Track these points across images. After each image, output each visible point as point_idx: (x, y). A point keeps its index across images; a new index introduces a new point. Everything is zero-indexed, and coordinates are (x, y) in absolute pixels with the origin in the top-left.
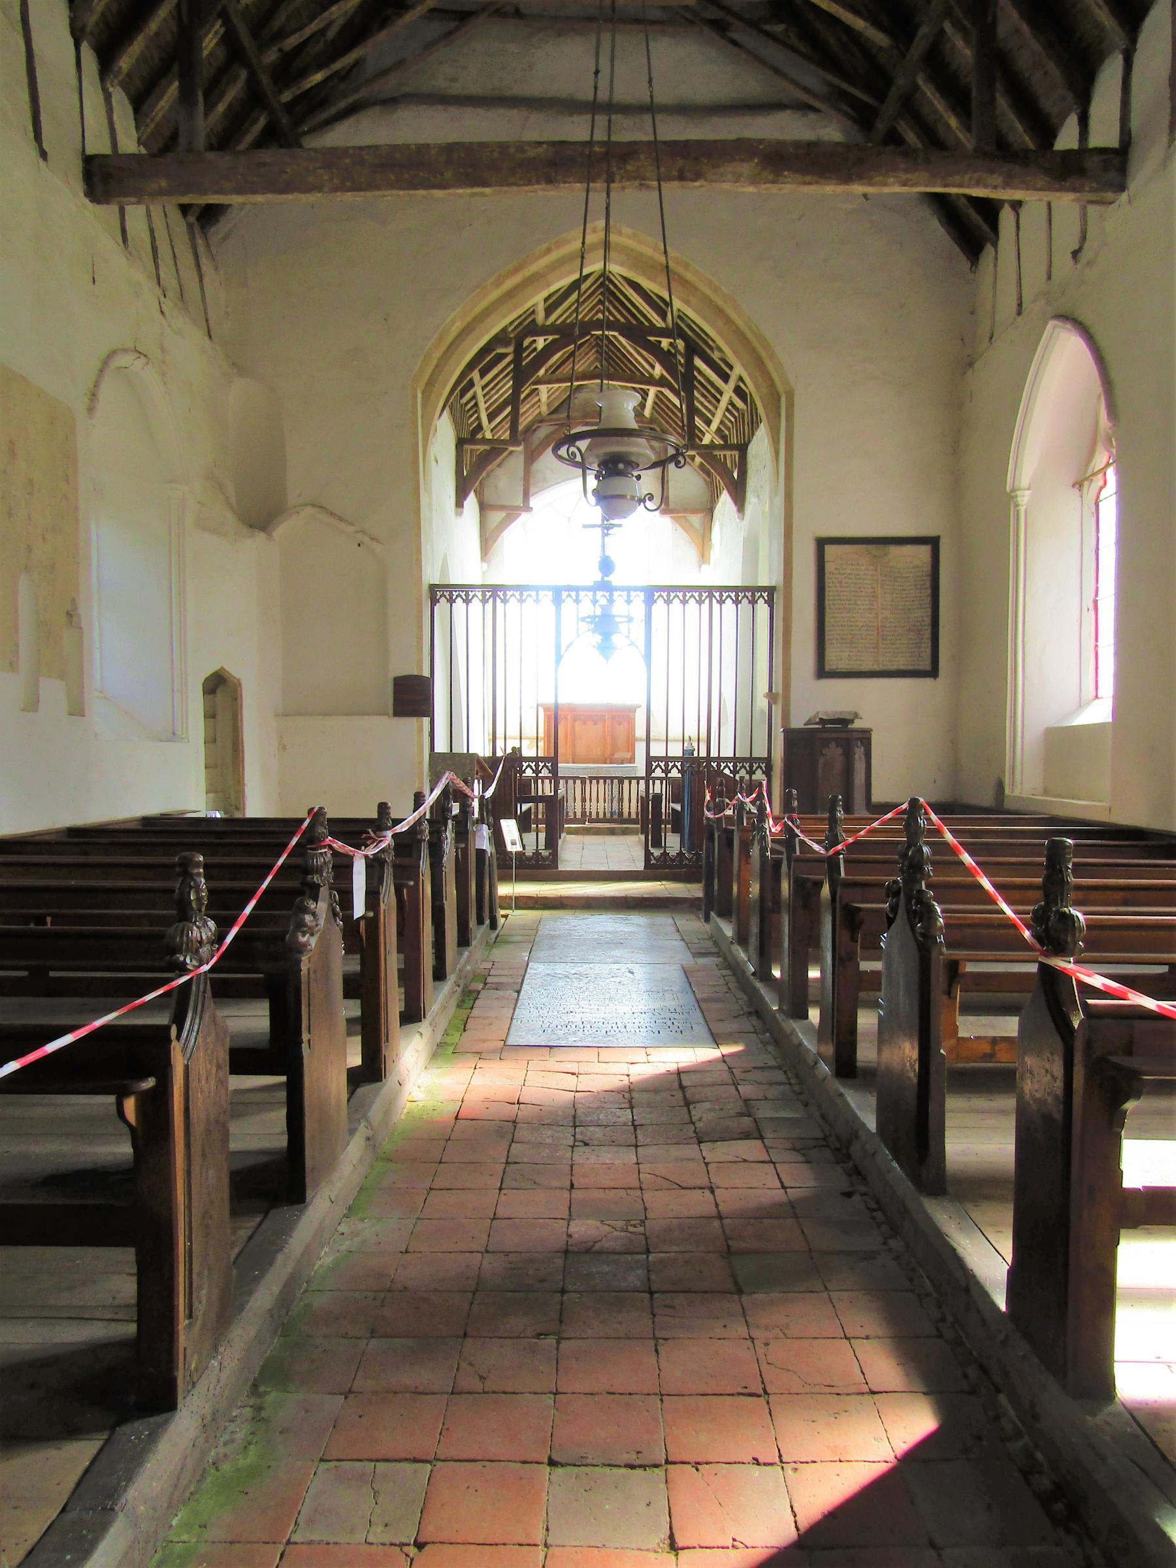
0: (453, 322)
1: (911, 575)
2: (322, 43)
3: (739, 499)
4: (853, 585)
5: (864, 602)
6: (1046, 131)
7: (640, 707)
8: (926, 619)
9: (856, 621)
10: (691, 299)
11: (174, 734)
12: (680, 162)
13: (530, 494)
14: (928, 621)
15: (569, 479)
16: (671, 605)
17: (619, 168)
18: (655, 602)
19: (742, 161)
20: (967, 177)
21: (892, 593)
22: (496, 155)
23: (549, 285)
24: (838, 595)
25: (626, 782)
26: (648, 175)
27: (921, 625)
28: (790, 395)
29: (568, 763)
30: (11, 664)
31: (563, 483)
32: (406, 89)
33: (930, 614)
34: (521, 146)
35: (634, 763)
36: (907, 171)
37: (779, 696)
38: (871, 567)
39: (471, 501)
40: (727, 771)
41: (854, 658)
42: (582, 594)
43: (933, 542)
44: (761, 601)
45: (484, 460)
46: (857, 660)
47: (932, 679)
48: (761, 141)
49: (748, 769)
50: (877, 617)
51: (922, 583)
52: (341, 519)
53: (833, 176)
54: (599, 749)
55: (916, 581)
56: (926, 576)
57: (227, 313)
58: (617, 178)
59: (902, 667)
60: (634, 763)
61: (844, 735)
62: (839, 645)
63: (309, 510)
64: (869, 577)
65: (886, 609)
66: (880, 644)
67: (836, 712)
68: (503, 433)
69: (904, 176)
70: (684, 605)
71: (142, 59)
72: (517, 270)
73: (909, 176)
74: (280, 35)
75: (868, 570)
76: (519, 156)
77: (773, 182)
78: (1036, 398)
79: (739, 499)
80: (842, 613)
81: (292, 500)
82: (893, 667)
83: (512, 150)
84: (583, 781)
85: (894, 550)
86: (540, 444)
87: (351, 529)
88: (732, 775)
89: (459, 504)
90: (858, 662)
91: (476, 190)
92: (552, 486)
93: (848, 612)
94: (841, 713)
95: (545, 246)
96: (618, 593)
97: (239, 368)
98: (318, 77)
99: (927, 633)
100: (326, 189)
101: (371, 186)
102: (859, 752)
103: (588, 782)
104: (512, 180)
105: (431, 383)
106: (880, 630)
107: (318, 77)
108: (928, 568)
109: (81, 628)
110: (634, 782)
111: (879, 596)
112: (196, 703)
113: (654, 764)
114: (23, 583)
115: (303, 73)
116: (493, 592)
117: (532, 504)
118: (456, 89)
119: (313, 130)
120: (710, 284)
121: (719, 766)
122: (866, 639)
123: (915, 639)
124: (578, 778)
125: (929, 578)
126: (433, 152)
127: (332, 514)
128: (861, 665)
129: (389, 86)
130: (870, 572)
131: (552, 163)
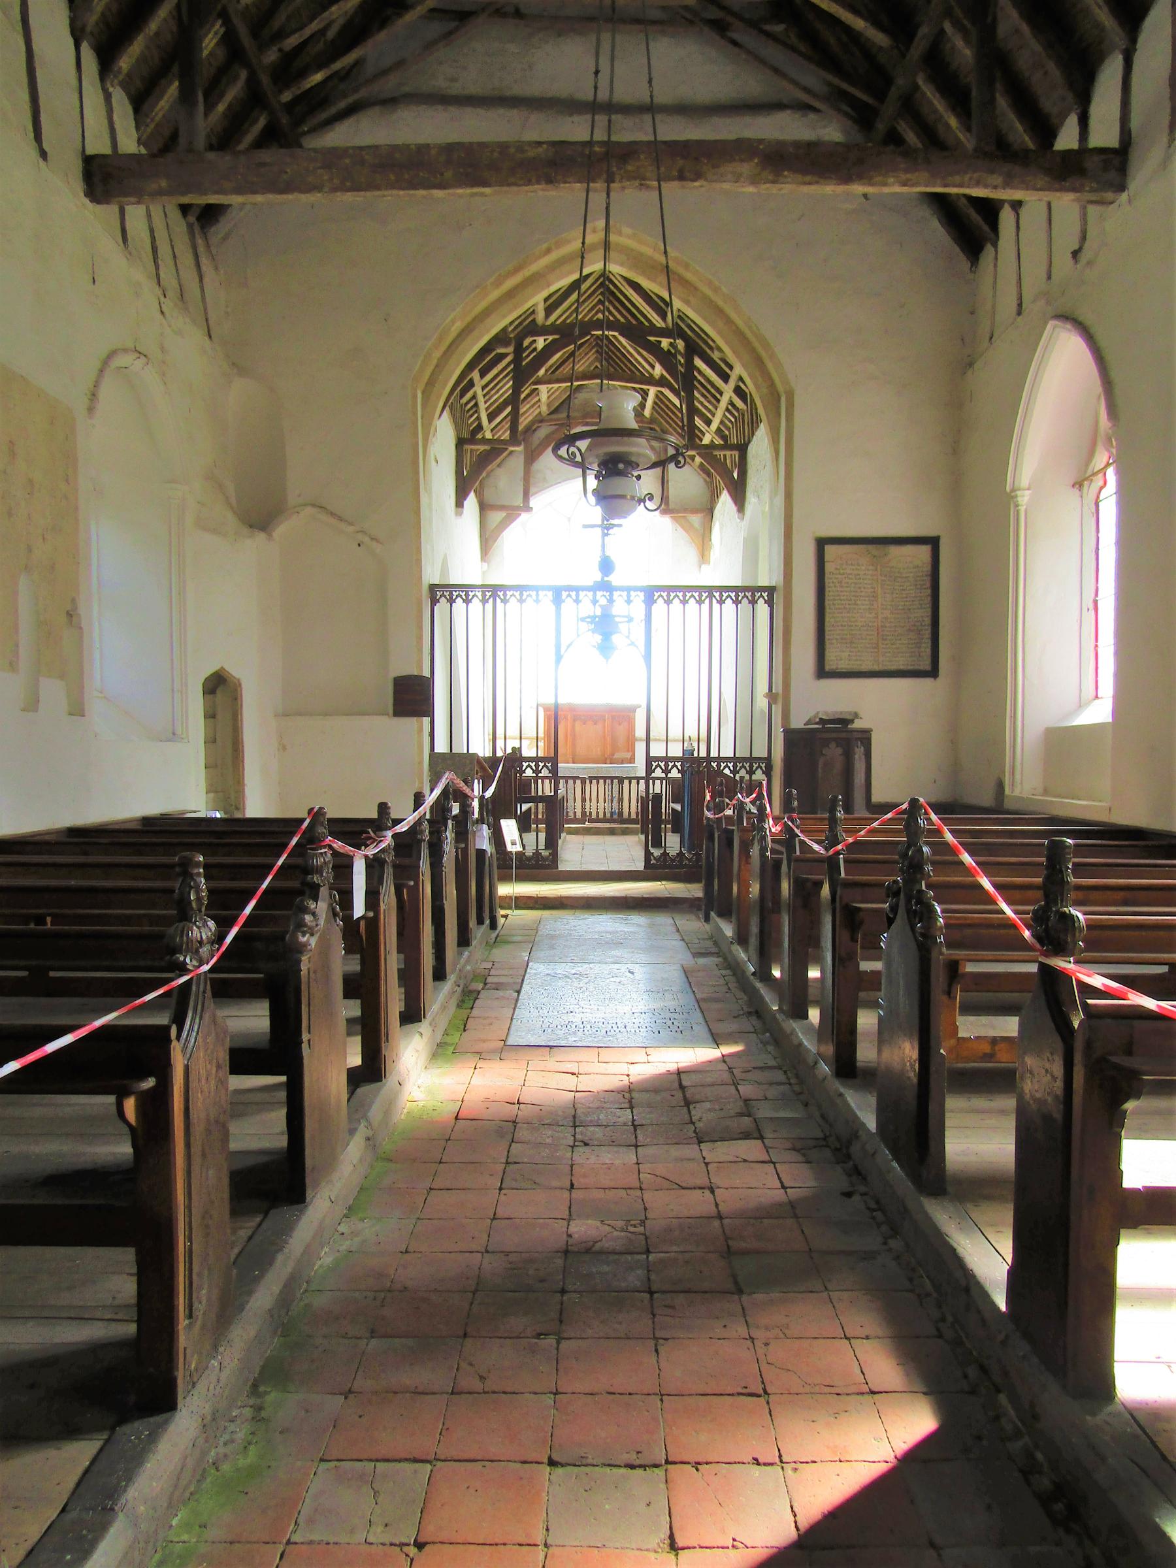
0: (453, 322)
1: (911, 575)
2: (322, 43)
3: (739, 499)
4: (853, 585)
5: (864, 602)
6: (1046, 131)
7: (640, 707)
8: (926, 619)
9: (856, 621)
10: (691, 299)
11: (174, 734)
12: (680, 162)
13: (530, 494)
14: (928, 621)
15: (569, 479)
16: (671, 605)
17: (619, 168)
18: (655, 602)
19: (742, 161)
20: (967, 177)
21: (892, 593)
22: (496, 155)
23: (549, 285)
24: (838, 595)
25: (626, 782)
26: (648, 175)
27: (921, 625)
28: (790, 395)
29: (568, 763)
30: (11, 664)
31: (563, 483)
32: (406, 89)
33: (930, 614)
34: (521, 146)
35: (634, 763)
36: (907, 171)
37: (779, 696)
38: (871, 567)
39: (471, 501)
40: (727, 771)
41: (854, 658)
42: (582, 594)
43: (933, 542)
44: (761, 601)
45: (484, 460)
46: (857, 660)
47: (932, 679)
48: (761, 141)
49: (748, 769)
50: (877, 617)
51: (922, 583)
52: (341, 519)
53: (833, 176)
54: (599, 749)
55: (916, 581)
56: (926, 576)
57: (227, 313)
58: (617, 178)
59: (902, 667)
60: (634, 763)
61: (844, 735)
62: (839, 645)
63: (309, 510)
64: (869, 577)
65: (886, 609)
66: (880, 644)
67: (836, 712)
68: (503, 433)
69: (904, 176)
70: (684, 605)
71: (142, 59)
72: (517, 270)
73: (909, 176)
74: (280, 35)
75: (868, 570)
76: (519, 156)
77: (773, 182)
78: (1036, 398)
79: (739, 499)
80: (842, 613)
81: (292, 500)
82: (893, 667)
83: (512, 150)
84: (583, 781)
85: (894, 550)
86: (540, 444)
87: (351, 529)
88: (732, 775)
89: (459, 504)
90: (858, 662)
91: (476, 190)
92: (552, 486)
93: (848, 612)
94: (841, 713)
95: (545, 246)
96: (618, 593)
97: (239, 368)
98: (318, 77)
99: (927, 633)
100: (326, 189)
101: (371, 186)
102: (859, 752)
103: (588, 782)
104: (512, 180)
105: (431, 383)
106: (880, 630)
107: (318, 77)
108: (928, 568)
109: (81, 628)
110: (634, 782)
111: (879, 596)
112: (196, 703)
113: (654, 764)
114: (23, 583)
115: (303, 73)
116: (493, 592)
117: (532, 504)
118: (456, 89)
119: (313, 130)
120: (710, 284)
121: (719, 766)
122: (866, 639)
123: (915, 639)
124: (578, 778)
125: (929, 578)
126: (433, 152)
127: (332, 514)
128: (861, 665)
129: (389, 86)
130: (870, 572)
131: (552, 163)
